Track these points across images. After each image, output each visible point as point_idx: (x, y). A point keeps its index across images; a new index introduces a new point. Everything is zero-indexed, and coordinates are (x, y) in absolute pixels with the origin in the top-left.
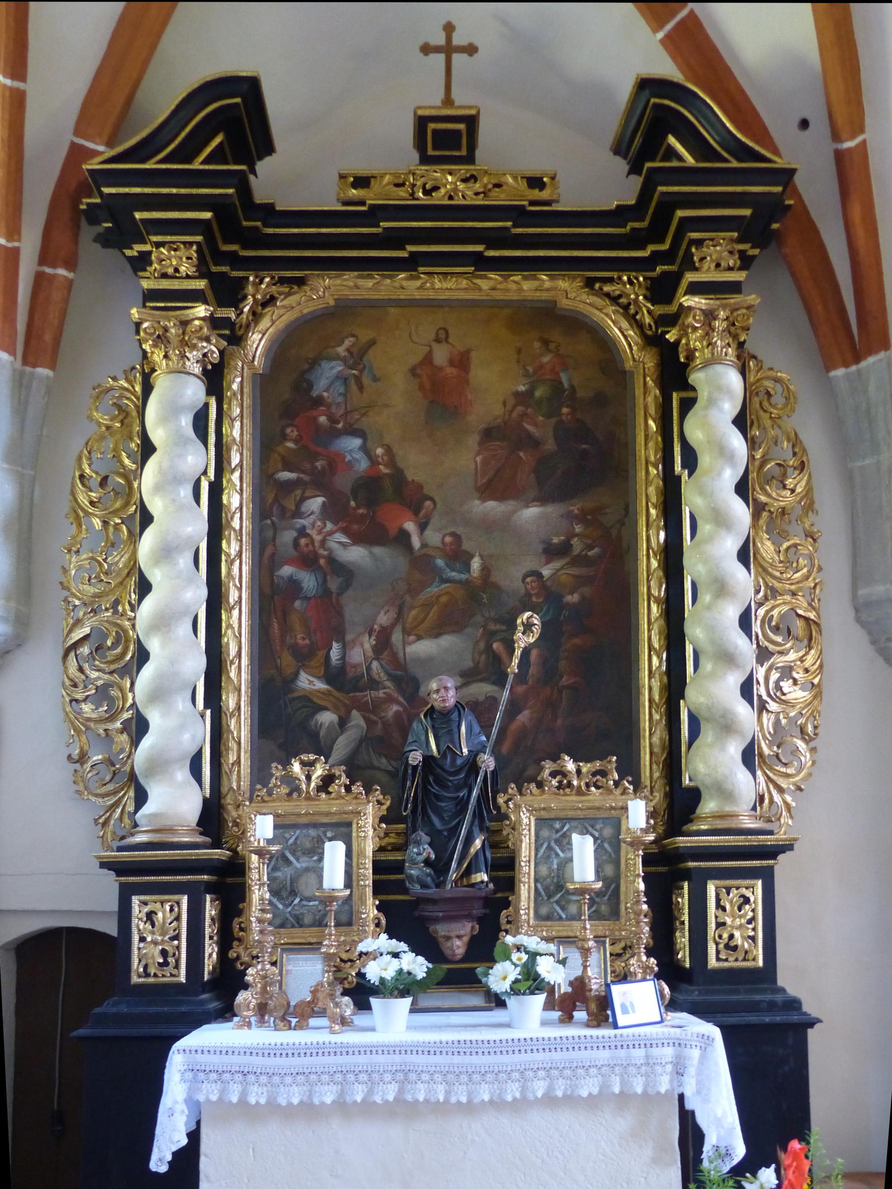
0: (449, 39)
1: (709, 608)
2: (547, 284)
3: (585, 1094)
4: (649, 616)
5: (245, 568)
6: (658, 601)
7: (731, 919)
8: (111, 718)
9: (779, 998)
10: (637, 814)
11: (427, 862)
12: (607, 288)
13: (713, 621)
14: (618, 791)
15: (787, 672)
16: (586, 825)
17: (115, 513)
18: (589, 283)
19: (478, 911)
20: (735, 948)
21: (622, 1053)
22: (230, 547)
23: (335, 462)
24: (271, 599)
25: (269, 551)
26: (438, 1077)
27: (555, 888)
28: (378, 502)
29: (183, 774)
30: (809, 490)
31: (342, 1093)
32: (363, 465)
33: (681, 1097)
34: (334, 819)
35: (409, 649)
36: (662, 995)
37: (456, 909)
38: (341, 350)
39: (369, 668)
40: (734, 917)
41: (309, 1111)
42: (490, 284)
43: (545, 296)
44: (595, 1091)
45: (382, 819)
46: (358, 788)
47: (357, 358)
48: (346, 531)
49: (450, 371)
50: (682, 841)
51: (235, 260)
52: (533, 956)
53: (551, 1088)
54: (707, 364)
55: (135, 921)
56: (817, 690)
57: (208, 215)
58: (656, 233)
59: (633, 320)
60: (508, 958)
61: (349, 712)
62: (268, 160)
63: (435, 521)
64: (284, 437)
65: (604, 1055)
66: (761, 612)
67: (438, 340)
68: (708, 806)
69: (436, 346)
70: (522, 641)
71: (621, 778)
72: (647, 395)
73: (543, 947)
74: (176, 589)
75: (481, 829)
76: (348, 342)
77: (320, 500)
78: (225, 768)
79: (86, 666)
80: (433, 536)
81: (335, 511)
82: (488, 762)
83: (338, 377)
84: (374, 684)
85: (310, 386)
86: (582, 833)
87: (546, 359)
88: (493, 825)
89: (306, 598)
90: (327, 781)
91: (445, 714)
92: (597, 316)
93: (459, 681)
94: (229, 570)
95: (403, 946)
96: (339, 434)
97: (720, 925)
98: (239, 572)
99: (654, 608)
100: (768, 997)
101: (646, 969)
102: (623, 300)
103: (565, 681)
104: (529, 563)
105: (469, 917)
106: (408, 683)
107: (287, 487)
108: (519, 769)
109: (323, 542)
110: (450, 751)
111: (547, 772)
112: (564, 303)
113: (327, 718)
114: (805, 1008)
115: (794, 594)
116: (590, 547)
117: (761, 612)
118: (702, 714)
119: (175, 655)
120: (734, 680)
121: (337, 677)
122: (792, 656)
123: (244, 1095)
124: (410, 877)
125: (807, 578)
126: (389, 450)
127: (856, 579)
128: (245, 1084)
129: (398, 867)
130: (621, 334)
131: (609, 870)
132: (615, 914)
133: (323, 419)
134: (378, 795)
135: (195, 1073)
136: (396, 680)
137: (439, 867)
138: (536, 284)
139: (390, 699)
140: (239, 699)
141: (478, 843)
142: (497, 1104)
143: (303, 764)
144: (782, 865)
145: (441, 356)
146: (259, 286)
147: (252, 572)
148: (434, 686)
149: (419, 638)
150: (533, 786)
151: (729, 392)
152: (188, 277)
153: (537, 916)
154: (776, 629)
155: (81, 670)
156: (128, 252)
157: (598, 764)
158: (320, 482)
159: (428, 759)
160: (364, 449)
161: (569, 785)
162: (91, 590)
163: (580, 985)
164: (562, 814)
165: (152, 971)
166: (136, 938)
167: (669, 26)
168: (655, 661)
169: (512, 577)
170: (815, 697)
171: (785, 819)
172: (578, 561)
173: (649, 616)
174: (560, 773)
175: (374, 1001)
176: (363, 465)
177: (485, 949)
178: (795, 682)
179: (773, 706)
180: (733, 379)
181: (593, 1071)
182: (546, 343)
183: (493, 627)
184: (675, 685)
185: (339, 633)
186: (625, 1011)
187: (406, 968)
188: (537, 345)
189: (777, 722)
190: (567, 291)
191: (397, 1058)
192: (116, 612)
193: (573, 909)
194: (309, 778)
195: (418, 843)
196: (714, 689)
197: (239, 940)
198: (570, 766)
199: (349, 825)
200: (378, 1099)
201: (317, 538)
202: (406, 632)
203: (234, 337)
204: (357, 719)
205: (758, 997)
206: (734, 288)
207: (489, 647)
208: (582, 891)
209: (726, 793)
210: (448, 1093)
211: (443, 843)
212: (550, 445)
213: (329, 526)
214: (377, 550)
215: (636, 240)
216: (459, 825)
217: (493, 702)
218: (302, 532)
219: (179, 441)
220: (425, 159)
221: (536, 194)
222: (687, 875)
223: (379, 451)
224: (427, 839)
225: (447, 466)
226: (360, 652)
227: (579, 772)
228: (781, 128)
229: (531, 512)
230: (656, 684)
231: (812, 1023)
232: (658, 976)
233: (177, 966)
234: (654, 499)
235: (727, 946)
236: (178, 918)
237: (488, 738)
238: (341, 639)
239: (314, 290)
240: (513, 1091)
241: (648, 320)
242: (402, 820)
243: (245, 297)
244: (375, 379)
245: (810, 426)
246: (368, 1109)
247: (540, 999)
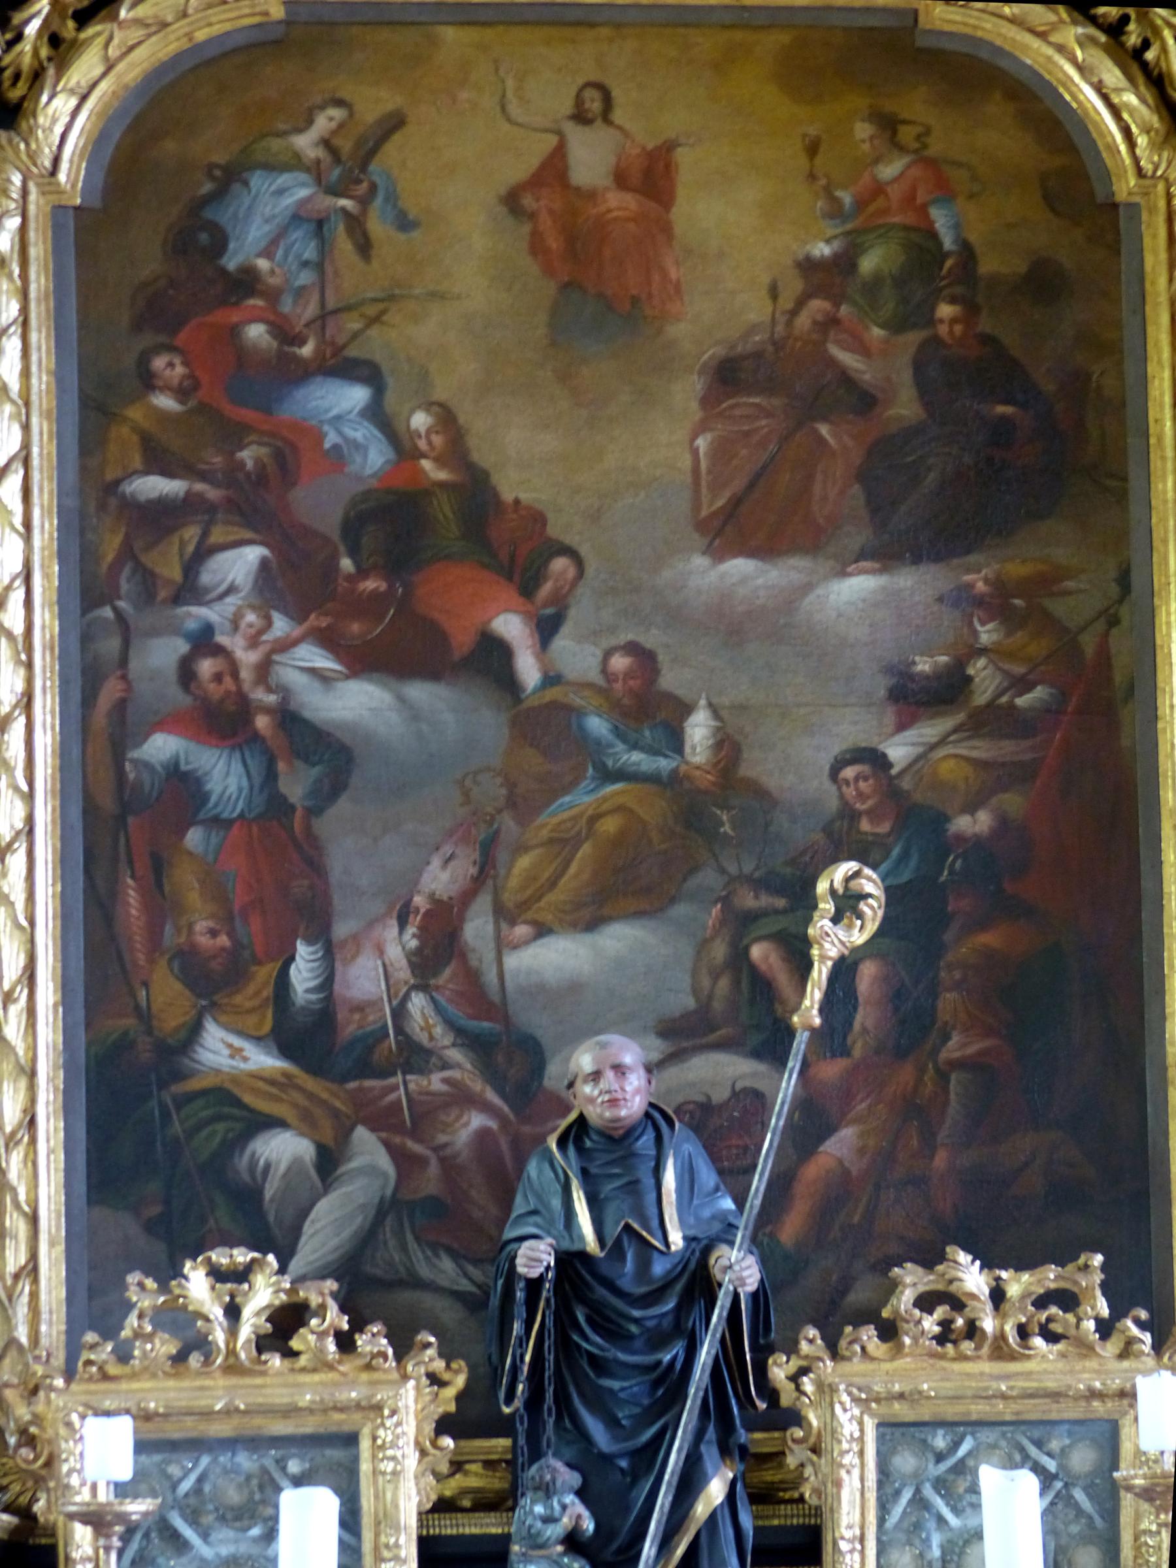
5: (45, 742)
14: (1111, 1348)
16: (1021, 1437)
23: (294, 453)
25: (110, 692)
28: (415, 559)
32: (376, 457)
34: (309, 1426)
35: (513, 961)
38: (306, 143)
39: (400, 1013)
45: (444, 1426)
47: (352, 164)
48: (327, 640)
49: (619, 203)
61: (344, 1135)
63: (579, 613)
64: (148, 381)
67: (581, 117)
69: (577, 136)
70: (831, 940)
71: (1119, 1311)
76: (323, 123)
77: (253, 554)
80: (577, 655)
81: (298, 582)
82: (740, 1269)
83: (296, 218)
84: (414, 1056)
85: (220, 243)
86: (1010, 1464)
87: (889, 171)
88: (759, 1440)
89: (217, 822)
90: (287, 1321)
91: (619, 1140)
93: (657, 1048)
96: (305, 373)
104: (852, 727)
106: (512, 1054)
107: (160, 518)
108: (828, 1291)
109: (264, 669)
110: (634, 1240)
111: (907, 1297)
113: (283, 1149)
116: (1023, 685)
121: (309, 1037)
126: (447, 419)
133: (256, 332)
134: (430, 1358)
136: (479, 1046)
141: (715, 1490)
143: (217, 1274)
148: (585, 1061)
149: (542, 931)
150: (868, 1334)
157: (1050, 1276)
158: (254, 505)
159: (571, 1262)
160: (376, 413)
161: (972, 1330)
164: (951, 1411)
169: (802, 766)
172: (991, 721)
176: (376, 457)
182: (888, 125)
183: (748, 900)
188: (863, 130)
194: (233, 1312)
195: (547, 1490)
198: (973, 1278)
199: (351, 1440)
201: (247, 658)
202: (504, 914)
204: (368, 1150)
207: (739, 956)
212: (905, 407)
213: (281, 625)
214: (419, 692)
217: (754, 1104)
218: (204, 642)
223: (420, 420)
226: (374, 969)
227: (998, 1296)
229: (853, 591)
237: (740, 1202)
238: (321, 933)
244: (405, 223)
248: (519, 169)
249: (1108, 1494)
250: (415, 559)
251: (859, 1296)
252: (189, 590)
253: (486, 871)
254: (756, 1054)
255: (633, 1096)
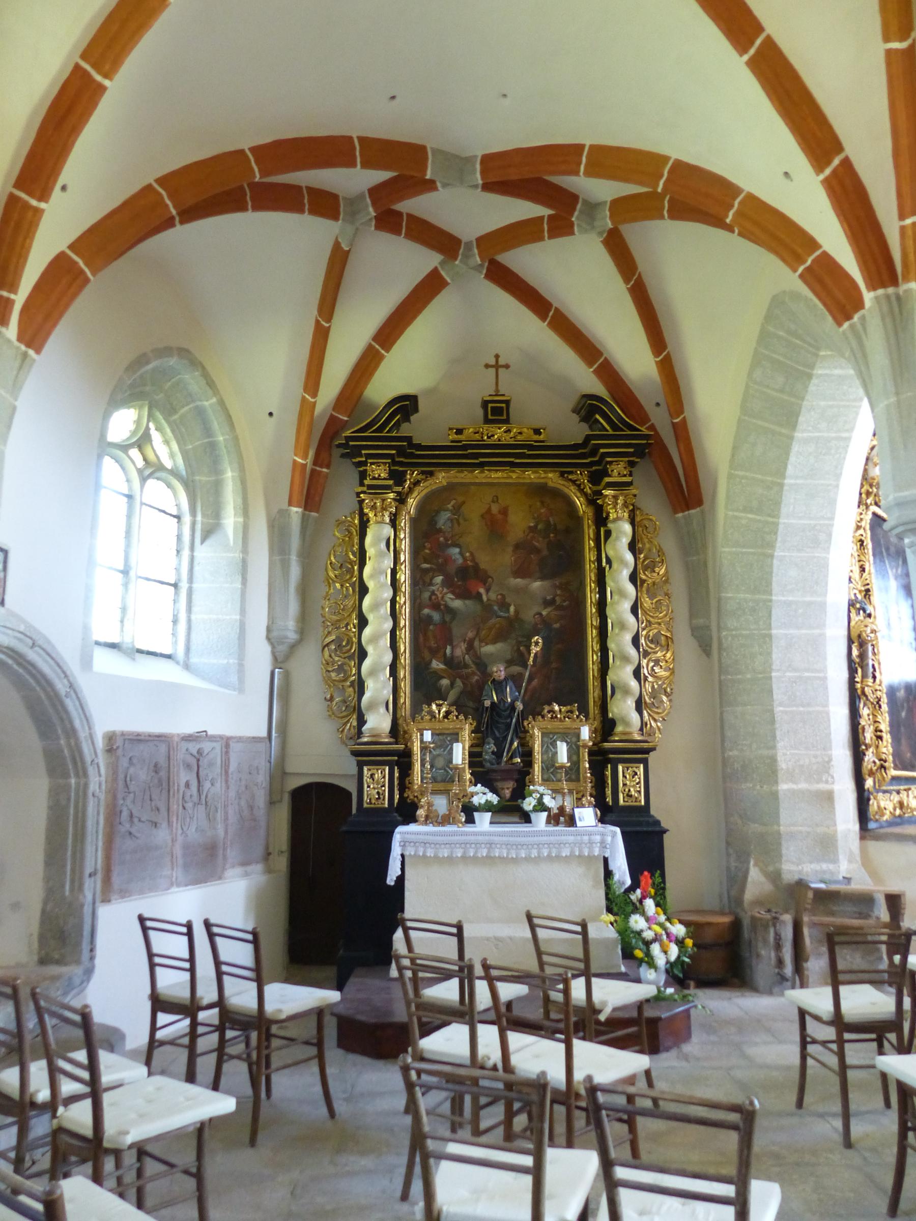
0: (497, 361)
1: (617, 635)
2: (543, 476)
3: (564, 855)
4: (592, 634)
5: (407, 610)
6: (596, 628)
7: (629, 783)
8: (345, 680)
9: (651, 820)
10: (585, 733)
11: (493, 753)
12: (570, 477)
13: (620, 640)
14: (578, 721)
15: (657, 662)
16: (564, 737)
17: (347, 581)
18: (562, 474)
19: (516, 776)
20: (631, 796)
21: (579, 838)
22: (401, 599)
23: (448, 560)
24: (419, 624)
25: (418, 601)
26: (504, 846)
27: (550, 766)
28: (467, 579)
29: (382, 710)
30: (667, 572)
31: (464, 853)
32: (460, 561)
33: (606, 860)
34: (451, 731)
35: (483, 649)
36: (596, 815)
37: (506, 775)
38: (450, 506)
39: (464, 658)
40: (631, 781)
41: (450, 860)
42: (515, 475)
43: (542, 481)
44: (568, 854)
45: (473, 732)
46: (461, 717)
47: (457, 510)
48: (453, 593)
49: (500, 517)
50: (607, 745)
51: (401, 464)
52: (542, 795)
53: (550, 852)
54: (615, 520)
55: (365, 778)
56: (672, 671)
57: (394, 452)
58: (594, 452)
59: (582, 491)
60: (531, 795)
61: (455, 680)
62: (416, 415)
63: (494, 588)
64: (424, 547)
65: (571, 839)
66: (644, 633)
67: (493, 501)
68: (619, 729)
69: (492, 505)
70: (535, 649)
71: (580, 714)
72: (589, 531)
73: (546, 791)
74: (378, 624)
75: (517, 737)
76: (453, 502)
77: (441, 578)
78: (399, 705)
79: (333, 655)
80: (493, 596)
81: (448, 583)
82: (519, 706)
83: (449, 519)
84: (466, 666)
85: (436, 523)
86: (562, 741)
87: (542, 511)
88: (521, 735)
89: (435, 625)
90: (448, 713)
91: (500, 683)
92: (566, 490)
93: (505, 665)
94: (400, 611)
95: (487, 790)
96: (448, 546)
97: (624, 785)
98: (405, 612)
99: (594, 631)
100: (647, 819)
101: (590, 803)
102: (578, 482)
103: (554, 665)
104: (536, 609)
105: (512, 779)
106: (482, 665)
107: (426, 571)
108: (534, 710)
109: (443, 597)
110: (502, 700)
111: (546, 711)
112: (550, 484)
113: (445, 682)
114: (662, 825)
115: (660, 624)
116: (565, 601)
117: (644, 633)
118: (616, 685)
119: (378, 654)
120: (630, 669)
121: (450, 662)
122: (659, 654)
123: (424, 852)
124: (485, 760)
125: (666, 615)
126: (472, 554)
127: (692, 615)
128: (425, 848)
129: (479, 755)
130: (579, 503)
131: (575, 758)
132: (578, 780)
133: (441, 539)
134: (470, 720)
135: (404, 844)
136: (476, 664)
137: (498, 755)
138: (538, 475)
139: (474, 673)
140: (404, 673)
141: (516, 744)
142: (528, 859)
143: (437, 705)
144: (652, 757)
145: (495, 509)
146: (412, 475)
147: (410, 612)
148: (495, 669)
149: (487, 644)
150: (540, 717)
151: (625, 534)
152: (385, 479)
153: (543, 779)
154: (652, 641)
155: (330, 656)
156: (354, 460)
157: (569, 707)
158: (441, 569)
159: (493, 703)
160: (461, 553)
161: (556, 717)
162: (335, 618)
163: (562, 809)
164: (553, 731)
165: (373, 801)
166: (366, 786)
167: (596, 366)
168: (595, 657)
169: (529, 616)
170: (671, 674)
171: (657, 734)
172: (560, 608)
173: (592, 634)
174: (552, 711)
175: (476, 814)
176: (460, 561)
177: (520, 793)
178: (661, 667)
179: (650, 679)
180: (627, 528)
181: (567, 845)
182: (542, 503)
183: (520, 639)
184: (604, 667)
185: (449, 640)
186: (580, 820)
187: (489, 799)
188: (538, 504)
189: (653, 687)
190: (552, 478)
191: (487, 838)
192: (347, 629)
193: (559, 776)
194: (439, 712)
195: (489, 743)
196: (621, 674)
197: (409, 788)
198: (557, 708)
199: (457, 734)
200: (479, 855)
201: (440, 596)
202: (481, 641)
203: (401, 500)
204: (459, 682)
205: (642, 819)
206: (630, 484)
207: (519, 649)
208: (562, 767)
209: (627, 723)
210: (508, 854)
211: (500, 744)
212: (545, 552)
213: (445, 590)
214: (467, 602)
215: (583, 456)
216: (507, 735)
217: (521, 676)
218: (433, 593)
219: (380, 555)
220: (487, 421)
221: (536, 437)
222: (609, 761)
223: (468, 554)
224: (493, 741)
225: (498, 562)
226: (460, 650)
227: (560, 710)
228: (649, 407)
229: (537, 584)
230: (596, 668)
231: (665, 831)
232: (595, 806)
233: (384, 799)
234: (593, 579)
235: (628, 795)
236: (384, 777)
237: (520, 693)
238: (451, 644)
239: (438, 479)
240: (534, 853)
241: (589, 491)
242: (482, 732)
243: (406, 481)
244: (465, 520)
245: (667, 541)
246: (475, 860)
247: (545, 814)
248: (484, 511)
249: (578, 747)
250: (467, 579)
251: (538, 709)
252: (431, 584)
253: (478, 631)
254: (521, 666)
255: (502, 675)
